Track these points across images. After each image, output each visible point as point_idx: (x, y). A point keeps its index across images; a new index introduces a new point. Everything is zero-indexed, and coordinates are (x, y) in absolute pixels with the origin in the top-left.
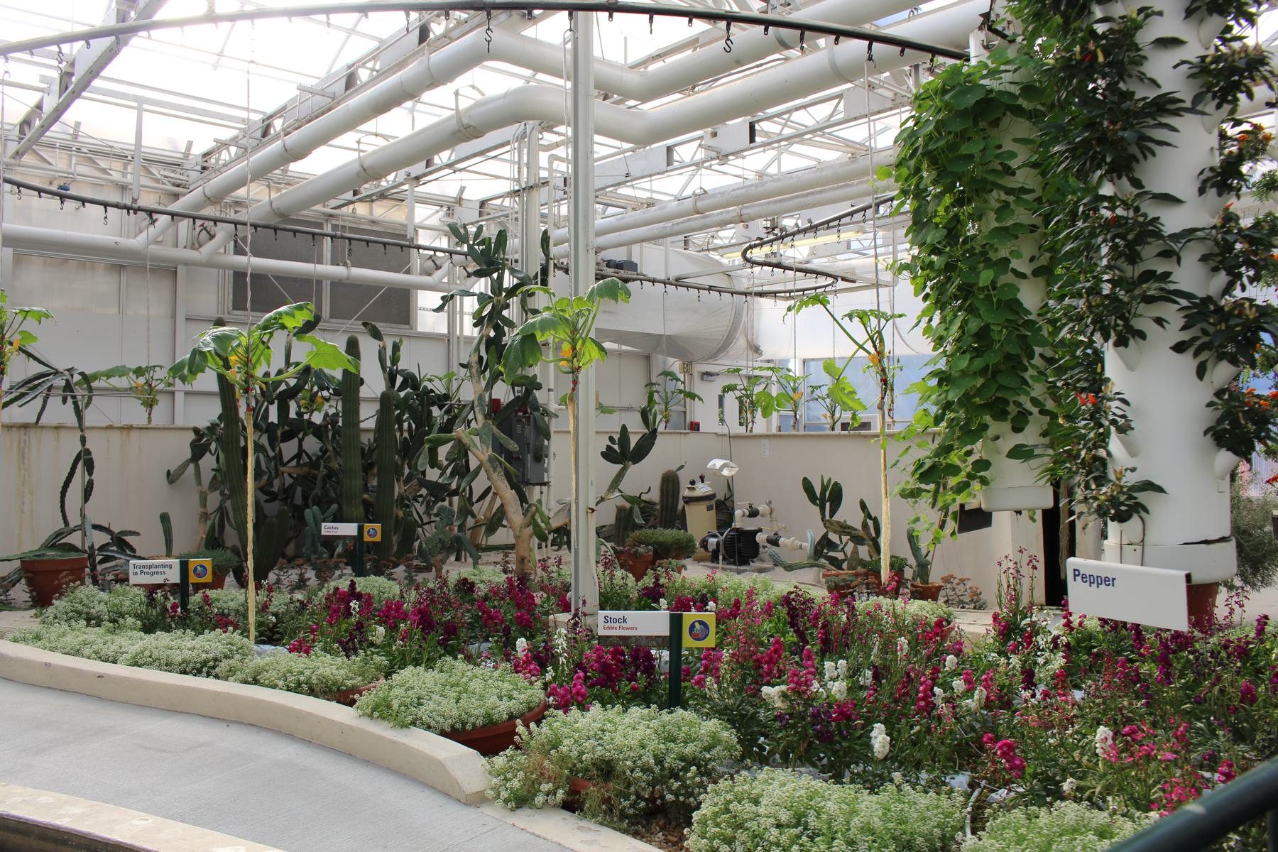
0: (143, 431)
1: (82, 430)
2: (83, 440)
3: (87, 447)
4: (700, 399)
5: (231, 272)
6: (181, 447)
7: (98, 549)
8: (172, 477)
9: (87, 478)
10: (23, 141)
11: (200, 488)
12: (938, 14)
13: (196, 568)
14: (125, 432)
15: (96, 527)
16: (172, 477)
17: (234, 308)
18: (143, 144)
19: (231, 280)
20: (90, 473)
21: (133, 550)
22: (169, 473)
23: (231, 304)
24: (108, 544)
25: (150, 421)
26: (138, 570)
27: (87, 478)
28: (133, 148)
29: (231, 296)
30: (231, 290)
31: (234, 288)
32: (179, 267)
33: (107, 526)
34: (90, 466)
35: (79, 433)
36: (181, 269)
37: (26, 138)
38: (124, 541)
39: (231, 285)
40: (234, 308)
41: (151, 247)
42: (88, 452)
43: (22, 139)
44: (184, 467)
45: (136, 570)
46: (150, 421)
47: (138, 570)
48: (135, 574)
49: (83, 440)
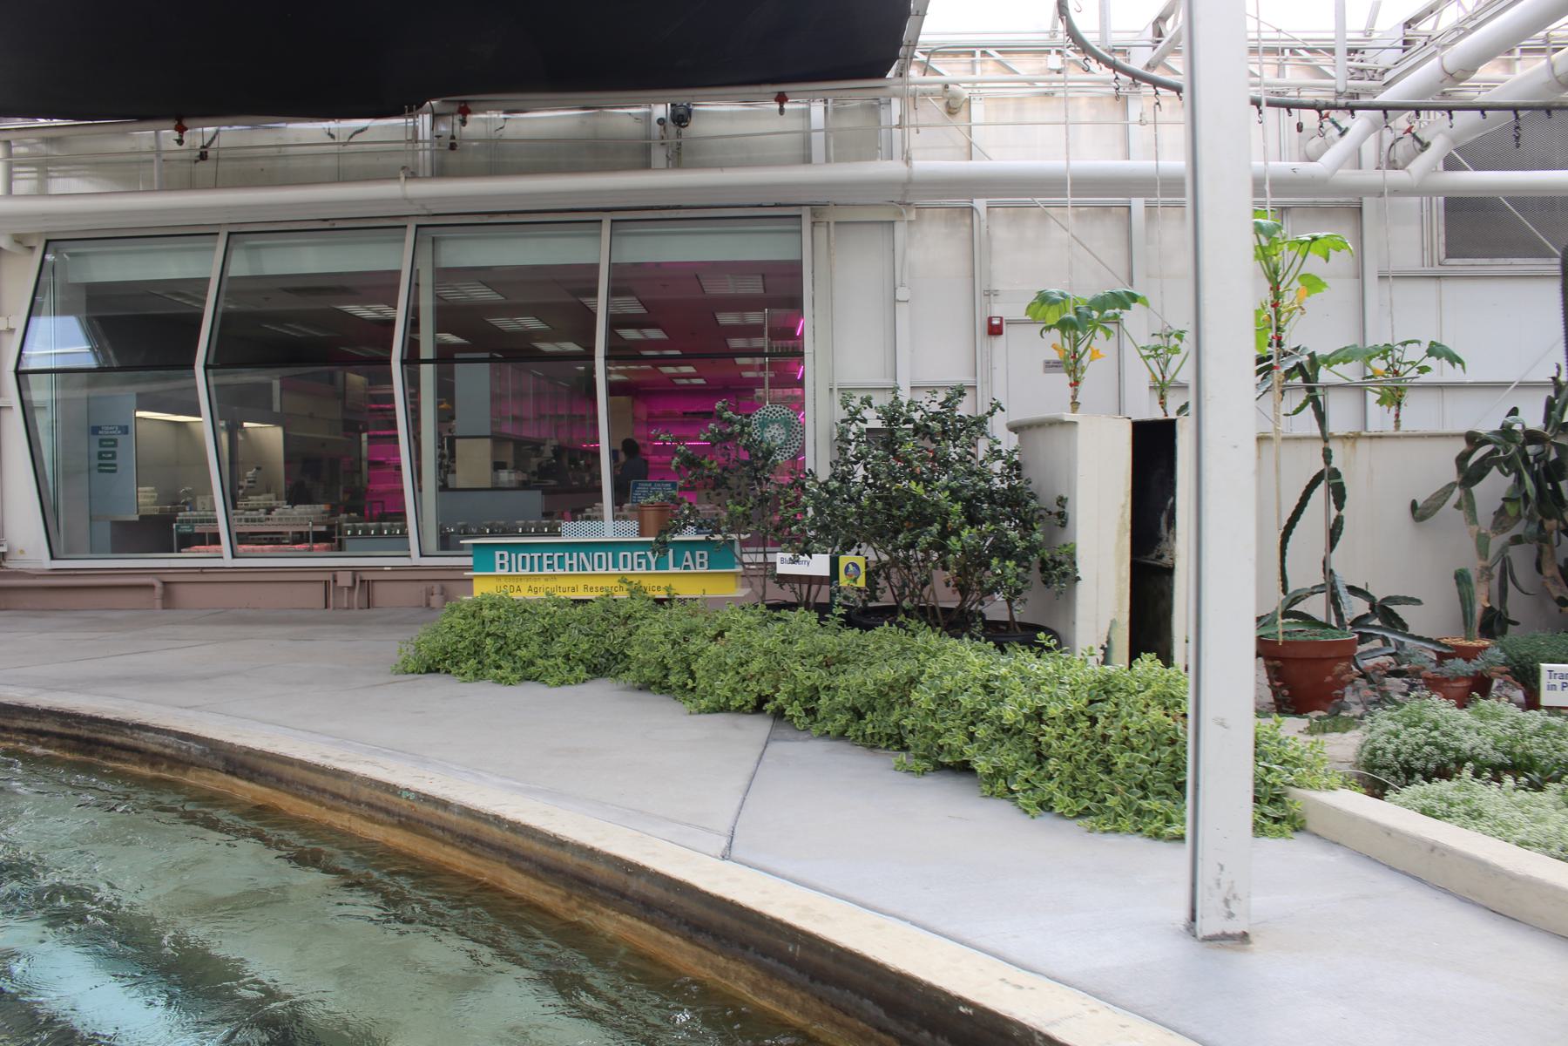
0: (1374, 440)
1: (1326, 441)
2: (1327, 455)
3: (1333, 465)
4: (1463, 368)
5: (1441, 199)
6: (1441, 467)
7: (1351, 624)
8: (1419, 513)
9: (1334, 513)
10: (1161, 45)
11: (1475, 528)
12: (229, 151)
13: (847, 568)
14: (1349, 443)
15: (1353, 590)
16: (1419, 513)
17: (1448, 256)
18: (1348, 27)
19: (1442, 213)
20: (1340, 506)
21: (1405, 626)
22: (1414, 505)
23: (1442, 249)
24: (1366, 616)
25: (1397, 426)
26: (1558, 682)
27: (1334, 513)
28: (1332, 36)
29: (1443, 238)
30: (1442, 229)
31: (1447, 225)
32: (1366, 200)
33: (1363, 587)
34: (1339, 495)
35: (1320, 445)
36: (1369, 204)
37: (1165, 41)
38: (1395, 616)
39: (1442, 221)
40: (1448, 256)
41: (1340, 171)
42: (1335, 474)
43: (1159, 42)
44: (1447, 490)
45: (1553, 682)
46: (1397, 426)
47: (1558, 682)
48: (1552, 687)
49: (1327, 455)
